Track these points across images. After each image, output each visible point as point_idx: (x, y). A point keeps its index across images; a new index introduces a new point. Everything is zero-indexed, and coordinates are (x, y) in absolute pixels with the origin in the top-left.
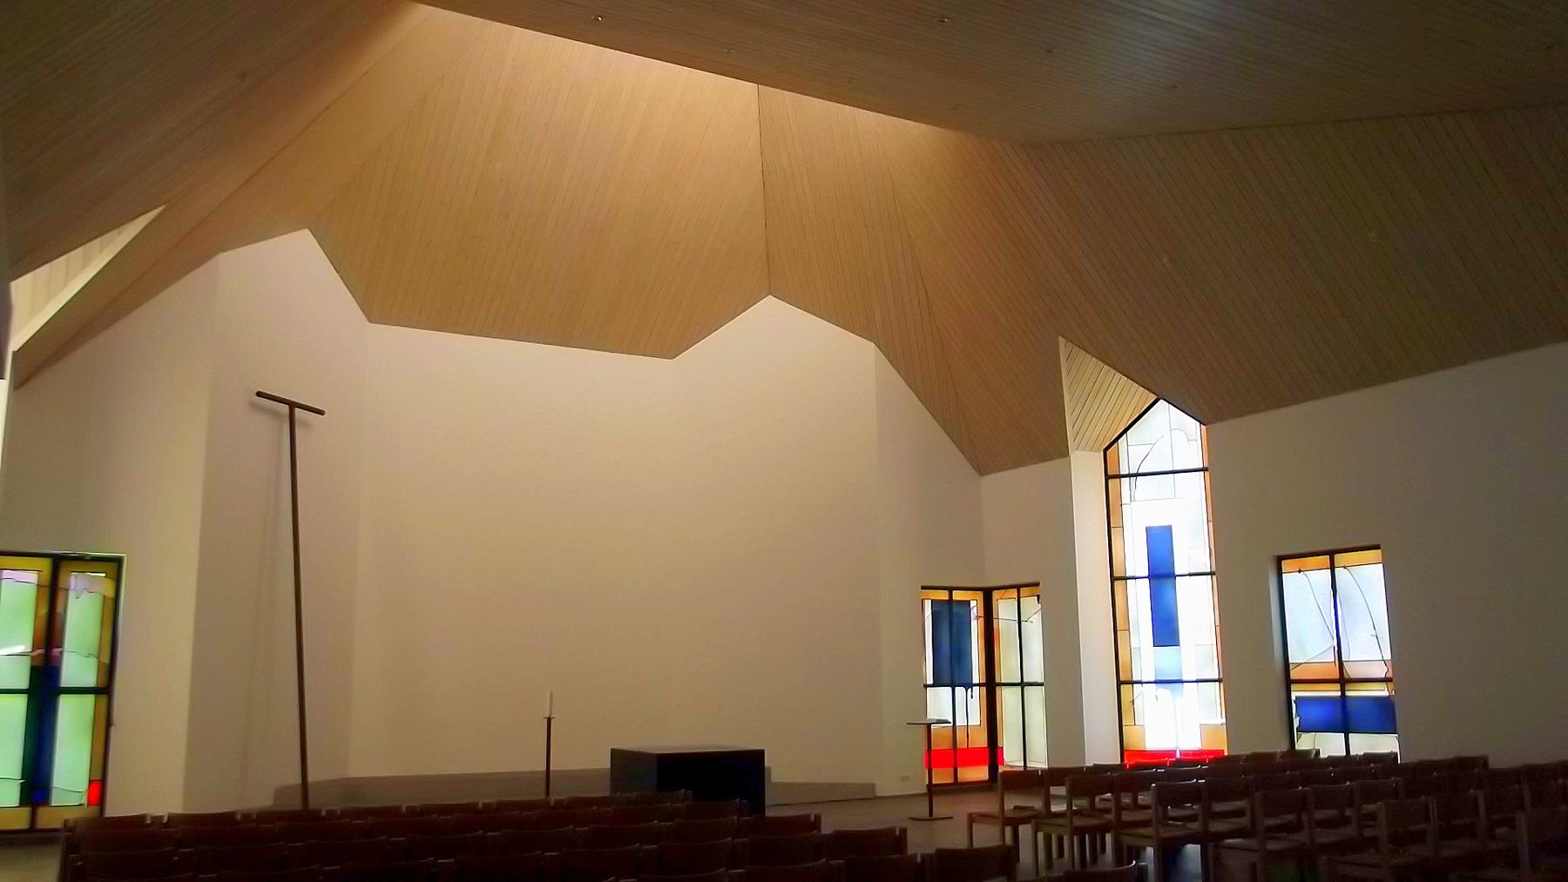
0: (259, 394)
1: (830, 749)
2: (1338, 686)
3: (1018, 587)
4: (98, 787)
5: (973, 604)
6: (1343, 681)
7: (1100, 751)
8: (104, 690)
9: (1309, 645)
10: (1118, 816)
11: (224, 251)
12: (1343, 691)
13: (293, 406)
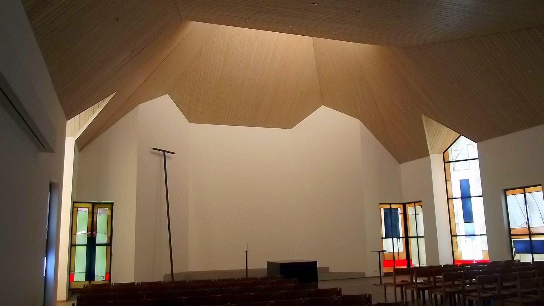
0: (153, 149)
1: (335, 260)
2: (528, 237)
3: (414, 203)
4: (109, 274)
5: (399, 209)
6: (530, 234)
7: (445, 260)
8: (109, 244)
9: (517, 221)
10: (435, 284)
12: (530, 238)
13: (165, 152)
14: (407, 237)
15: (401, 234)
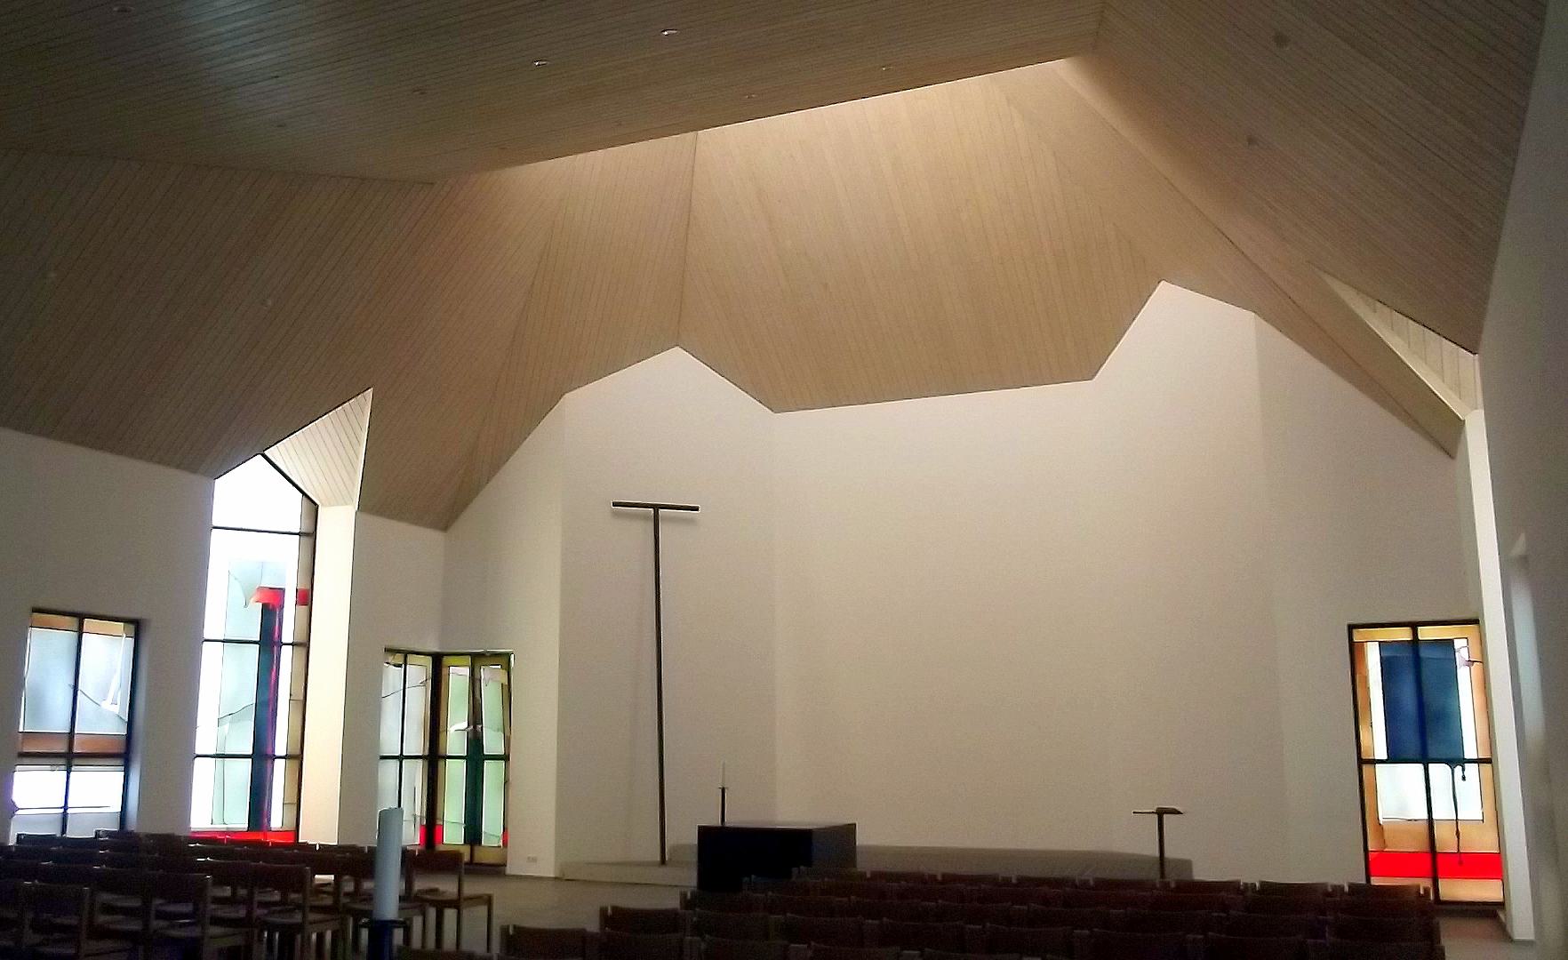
0: (615, 504)
5: (1458, 644)
13: (656, 507)
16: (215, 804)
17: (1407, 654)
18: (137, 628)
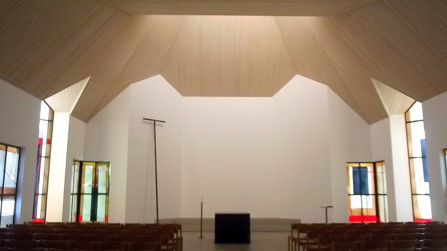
4: (106, 218)
11: (300, 74)
13: (155, 121)
14: (376, 194)
15: (371, 190)
16: (54, 210)
17: (357, 170)
18: (20, 150)
